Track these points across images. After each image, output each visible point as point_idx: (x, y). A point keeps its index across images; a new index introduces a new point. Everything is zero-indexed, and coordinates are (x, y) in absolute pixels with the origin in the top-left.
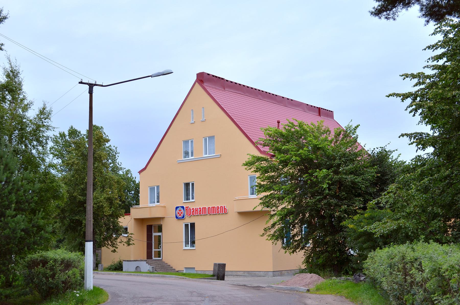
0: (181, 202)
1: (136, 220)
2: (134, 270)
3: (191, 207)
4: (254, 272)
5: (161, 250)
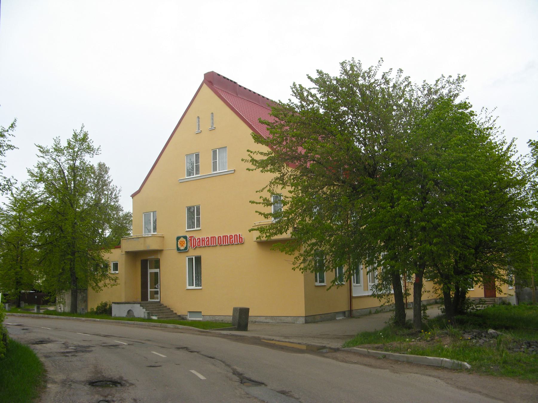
0: (183, 230)
1: (127, 253)
2: (124, 314)
3: (197, 236)
4: (280, 318)
5: (159, 290)
